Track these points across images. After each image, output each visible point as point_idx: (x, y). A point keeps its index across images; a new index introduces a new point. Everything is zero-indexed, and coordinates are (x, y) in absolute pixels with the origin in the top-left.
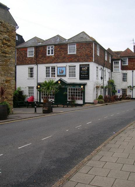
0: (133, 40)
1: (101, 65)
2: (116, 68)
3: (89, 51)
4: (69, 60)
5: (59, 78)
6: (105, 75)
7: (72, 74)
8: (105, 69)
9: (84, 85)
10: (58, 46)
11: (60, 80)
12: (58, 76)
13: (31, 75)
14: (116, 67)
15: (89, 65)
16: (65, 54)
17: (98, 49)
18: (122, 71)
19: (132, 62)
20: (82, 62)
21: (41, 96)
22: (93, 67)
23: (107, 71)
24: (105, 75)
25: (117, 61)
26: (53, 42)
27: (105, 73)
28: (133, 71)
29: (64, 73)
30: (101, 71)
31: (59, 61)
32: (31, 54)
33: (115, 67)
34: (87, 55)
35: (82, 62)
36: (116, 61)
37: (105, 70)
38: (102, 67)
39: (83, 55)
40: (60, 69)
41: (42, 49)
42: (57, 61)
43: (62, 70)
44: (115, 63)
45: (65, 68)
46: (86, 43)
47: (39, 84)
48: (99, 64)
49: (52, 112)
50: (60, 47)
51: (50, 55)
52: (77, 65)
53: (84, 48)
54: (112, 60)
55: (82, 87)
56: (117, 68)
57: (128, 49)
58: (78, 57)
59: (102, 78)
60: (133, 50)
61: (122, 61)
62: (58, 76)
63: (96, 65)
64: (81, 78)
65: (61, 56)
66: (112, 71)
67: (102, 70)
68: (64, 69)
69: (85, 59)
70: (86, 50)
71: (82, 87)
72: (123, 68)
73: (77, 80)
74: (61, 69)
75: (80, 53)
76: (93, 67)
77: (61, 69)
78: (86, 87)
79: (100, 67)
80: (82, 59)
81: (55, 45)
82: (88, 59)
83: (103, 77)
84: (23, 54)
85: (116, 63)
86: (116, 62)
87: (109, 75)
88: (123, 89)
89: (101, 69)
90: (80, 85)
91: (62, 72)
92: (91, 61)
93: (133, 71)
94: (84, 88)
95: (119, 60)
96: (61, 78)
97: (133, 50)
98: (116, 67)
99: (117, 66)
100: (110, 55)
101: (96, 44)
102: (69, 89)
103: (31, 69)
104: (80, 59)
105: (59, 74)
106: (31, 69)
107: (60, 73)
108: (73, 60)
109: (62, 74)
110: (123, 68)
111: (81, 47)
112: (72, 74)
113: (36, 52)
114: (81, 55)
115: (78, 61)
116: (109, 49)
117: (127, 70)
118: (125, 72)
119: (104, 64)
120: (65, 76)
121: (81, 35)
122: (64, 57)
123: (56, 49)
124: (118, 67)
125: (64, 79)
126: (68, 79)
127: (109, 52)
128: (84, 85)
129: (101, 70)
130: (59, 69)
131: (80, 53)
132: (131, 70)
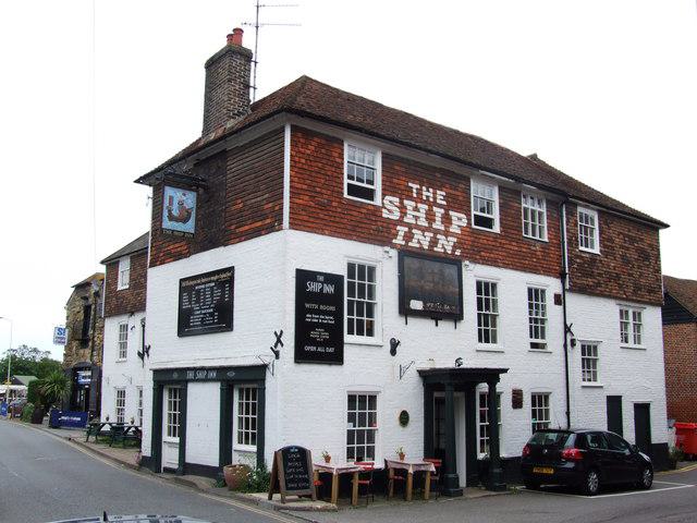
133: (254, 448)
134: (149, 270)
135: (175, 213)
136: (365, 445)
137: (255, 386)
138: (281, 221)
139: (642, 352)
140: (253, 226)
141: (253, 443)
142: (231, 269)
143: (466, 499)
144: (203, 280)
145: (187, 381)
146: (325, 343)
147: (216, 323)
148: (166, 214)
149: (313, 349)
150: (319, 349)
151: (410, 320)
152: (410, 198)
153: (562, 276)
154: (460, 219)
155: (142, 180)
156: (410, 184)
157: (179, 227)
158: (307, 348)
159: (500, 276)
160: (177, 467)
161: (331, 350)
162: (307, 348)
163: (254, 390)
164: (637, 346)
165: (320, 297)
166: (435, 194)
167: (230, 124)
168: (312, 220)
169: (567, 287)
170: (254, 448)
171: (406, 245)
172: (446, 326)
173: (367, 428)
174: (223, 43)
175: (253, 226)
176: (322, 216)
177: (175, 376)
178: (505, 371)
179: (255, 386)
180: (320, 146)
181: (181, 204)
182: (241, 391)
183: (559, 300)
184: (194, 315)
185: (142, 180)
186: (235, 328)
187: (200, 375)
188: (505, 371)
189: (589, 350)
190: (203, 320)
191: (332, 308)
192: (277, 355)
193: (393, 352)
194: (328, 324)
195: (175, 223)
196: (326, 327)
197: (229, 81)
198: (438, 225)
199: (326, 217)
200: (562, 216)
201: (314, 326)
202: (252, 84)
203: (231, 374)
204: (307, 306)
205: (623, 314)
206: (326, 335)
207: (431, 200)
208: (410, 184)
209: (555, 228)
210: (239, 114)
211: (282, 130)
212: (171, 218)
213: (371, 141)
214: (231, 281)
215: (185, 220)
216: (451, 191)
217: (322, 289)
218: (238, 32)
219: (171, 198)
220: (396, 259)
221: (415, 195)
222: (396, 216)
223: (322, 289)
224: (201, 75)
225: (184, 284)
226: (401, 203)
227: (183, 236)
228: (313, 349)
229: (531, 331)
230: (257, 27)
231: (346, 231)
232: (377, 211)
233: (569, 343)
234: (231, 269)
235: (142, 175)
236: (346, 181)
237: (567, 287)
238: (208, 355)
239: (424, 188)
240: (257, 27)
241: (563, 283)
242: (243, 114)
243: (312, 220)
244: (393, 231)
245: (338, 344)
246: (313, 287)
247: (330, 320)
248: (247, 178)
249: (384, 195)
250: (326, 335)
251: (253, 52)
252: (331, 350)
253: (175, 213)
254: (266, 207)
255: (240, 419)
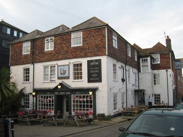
0: (165, 33)
1: (121, 62)
2: (144, 68)
3: (99, 41)
4: (73, 55)
5: (60, 81)
6: (129, 76)
7: (78, 76)
8: (128, 67)
9: (94, 90)
10: (59, 37)
11: (60, 84)
12: (59, 78)
13: (27, 79)
14: (145, 66)
15: (100, 60)
16: (67, 47)
17: (115, 38)
18: (153, 71)
19: (165, 58)
20: (90, 57)
21: (38, 106)
22: (106, 62)
23: (132, 71)
24: (129, 76)
25: (145, 58)
26: (53, 33)
27: (129, 74)
28: (167, 71)
29: (66, 75)
30: (122, 70)
31: (60, 57)
32: (26, 48)
33: (143, 66)
34: (97, 46)
35: (91, 56)
36: (143, 59)
37: (129, 70)
38: (124, 65)
39: (92, 47)
40: (61, 69)
41: (39, 43)
42: (57, 57)
43: (63, 69)
44: (142, 61)
45: (67, 67)
46: (95, 29)
47: (35, 90)
48: (118, 60)
49: (151, 102)
50: (61, 38)
51: (49, 49)
52: (84, 61)
53: (94, 36)
54: (139, 57)
55: (91, 93)
56: (146, 67)
57: (159, 42)
58: (85, 49)
59: (123, 80)
60: (166, 46)
61: (152, 58)
62: (59, 78)
63: (112, 61)
64: (89, 81)
65: (62, 50)
66: (139, 71)
67: (124, 69)
68: (66, 68)
69: (94, 52)
70: (95, 39)
71: (91, 93)
72: (154, 67)
73: (84, 83)
74: (62, 68)
75: (87, 44)
76: (106, 62)
77: (62, 68)
78: (97, 93)
79: (119, 65)
80: (91, 52)
81: (55, 36)
82: (98, 51)
83: (125, 78)
84: (18, 51)
85: (145, 61)
86: (145, 60)
87: (136, 77)
88: (155, 95)
89: (122, 67)
90: (87, 90)
91: (64, 73)
92: (103, 54)
93: (167, 71)
94: (94, 94)
95: (147, 56)
96: (62, 81)
97: (166, 46)
98: (145, 66)
99: (146, 64)
100: (135, 51)
101: (111, 31)
102: (52, 96)
103: (27, 71)
104: (88, 52)
105: (60, 76)
106: (27, 71)
107: (61, 74)
108: (78, 54)
109: (64, 76)
110: (154, 67)
111: (88, 35)
112: (78, 76)
113: (33, 47)
114: (89, 47)
115: (85, 56)
116: (135, 44)
117: (159, 69)
118: (156, 72)
119: (126, 61)
120: (68, 78)
121: (92, 21)
122: (67, 52)
123: (56, 42)
124: (147, 66)
125: (67, 82)
126: (72, 83)
127: (135, 48)
128: (94, 90)
129: (122, 68)
130: (60, 68)
131: (87, 44)
132: (165, 69)
135: (62, 73)
136: (79, 76)
143: (11, 73)
146: (96, 77)
149: (93, 79)
150: (94, 79)
158: (91, 79)
161: (98, 79)
162: (91, 79)
165: (95, 66)
195: (62, 75)
196: (96, 73)
201: (93, 73)
204: (91, 69)
205: (114, 66)
206: (96, 75)
228: (93, 79)
229: (116, 66)
236: (93, 109)
246: (92, 64)
247: (97, 71)
250: (96, 75)
252: (98, 79)
253: (62, 73)
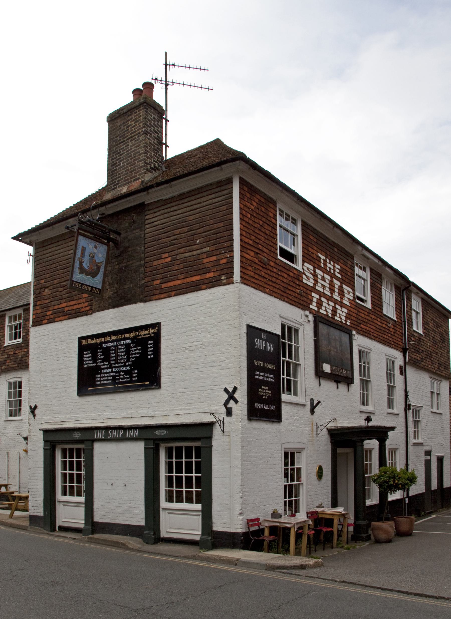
133: (199, 507)
134: (34, 332)
137: (198, 444)
138: (230, 275)
139: (440, 415)
140: (187, 280)
141: (197, 502)
142: (157, 326)
144: (114, 338)
145: (93, 441)
147: (135, 381)
148: (77, 265)
151: (322, 382)
152: (320, 268)
153: (404, 351)
154: (349, 292)
155: (20, 237)
156: (320, 255)
157: (88, 280)
159: (372, 347)
160: (82, 526)
163: (198, 449)
164: (437, 411)
166: (334, 266)
167: (148, 177)
168: (257, 276)
169: (407, 360)
170: (82, 499)
171: (318, 312)
172: (343, 387)
173: (296, 483)
174: (129, 99)
175: (187, 280)
176: (263, 274)
177: (77, 436)
178: (392, 429)
179: (198, 444)
180: (260, 203)
181: (92, 257)
182: (64, 452)
183: (403, 371)
184: (101, 373)
185: (20, 237)
186: (162, 385)
187: (114, 434)
188: (392, 429)
189: (416, 413)
190: (114, 379)
191: (273, 367)
192: (229, 412)
193: (312, 411)
194: (270, 382)
197: (146, 133)
198: (336, 296)
199: (266, 276)
200: (403, 299)
202: (164, 141)
203: (160, 433)
207: (332, 272)
208: (320, 255)
209: (399, 309)
210: (155, 169)
211: (230, 181)
212: (82, 270)
213: (306, 208)
214: (157, 338)
215: (94, 274)
216: (345, 267)
217: (265, 347)
218: (149, 86)
219: (84, 249)
220: (312, 324)
221: (322, 266)
222: (311, 283)
223: (265, 347)
224: (105, 127)
225: (84, 343)
226: (314, 271)
227: (91, 290)
230: (167, 85)
231: (279, 292)
232: (299, 275)
233: (407, 407)
234: (157, 326)
235: (22, 231)
237: (407, 360)
238: (124, 414)
239: (328, 260)
240: (167, 85)
241: (404, 356)
242: (159, 170)
243: (257, 276)
244: (310, 297)
245: (278, 402)
246: (259, 344)
247: (271, 378)
248: (178, 231)
249: (304, 261)
251: (164, 109)
252: (272, 408)
253: (86, 265)
254: (205, 261)
255: (64, 475)
